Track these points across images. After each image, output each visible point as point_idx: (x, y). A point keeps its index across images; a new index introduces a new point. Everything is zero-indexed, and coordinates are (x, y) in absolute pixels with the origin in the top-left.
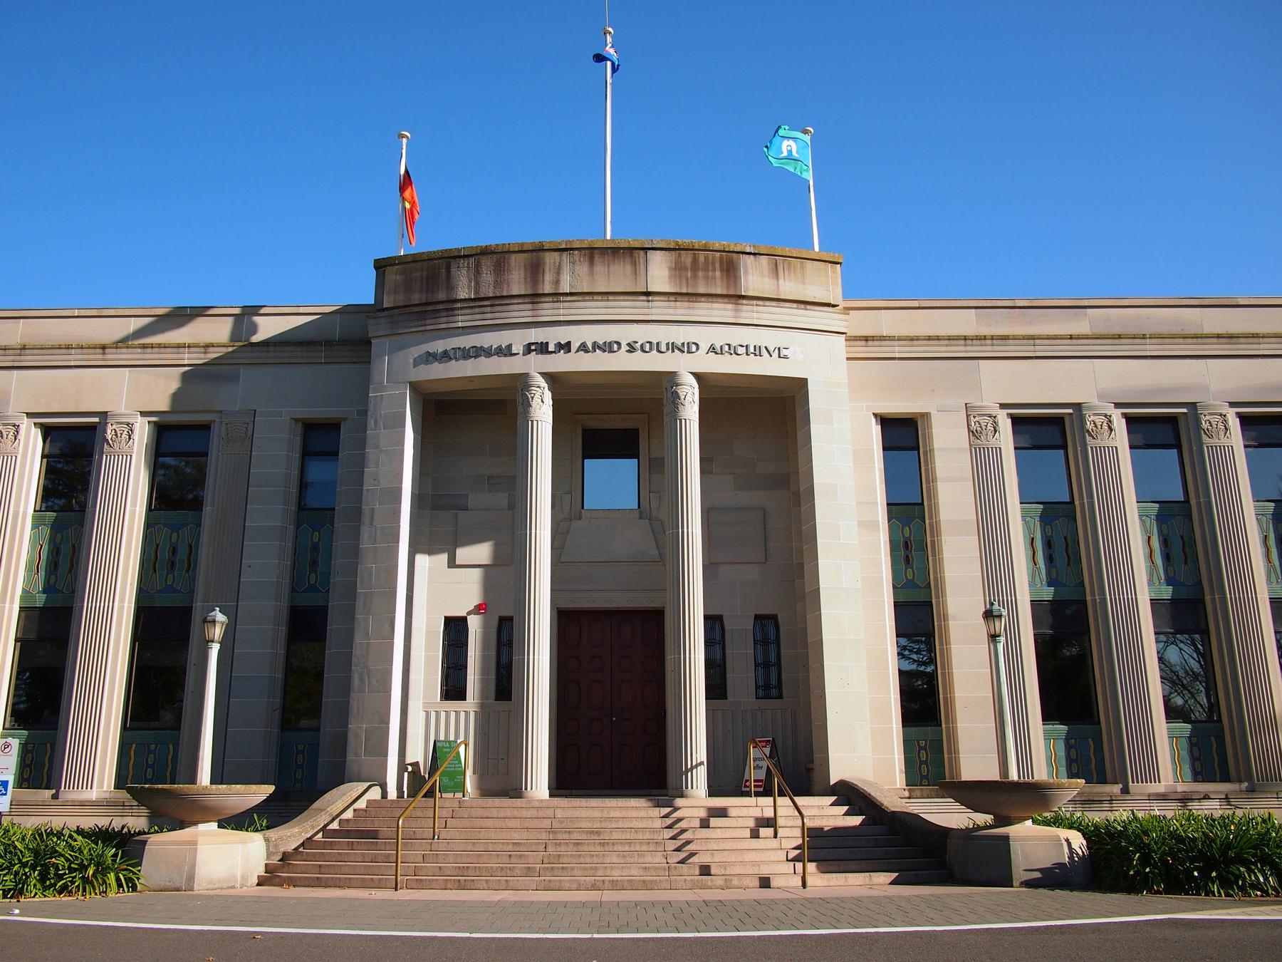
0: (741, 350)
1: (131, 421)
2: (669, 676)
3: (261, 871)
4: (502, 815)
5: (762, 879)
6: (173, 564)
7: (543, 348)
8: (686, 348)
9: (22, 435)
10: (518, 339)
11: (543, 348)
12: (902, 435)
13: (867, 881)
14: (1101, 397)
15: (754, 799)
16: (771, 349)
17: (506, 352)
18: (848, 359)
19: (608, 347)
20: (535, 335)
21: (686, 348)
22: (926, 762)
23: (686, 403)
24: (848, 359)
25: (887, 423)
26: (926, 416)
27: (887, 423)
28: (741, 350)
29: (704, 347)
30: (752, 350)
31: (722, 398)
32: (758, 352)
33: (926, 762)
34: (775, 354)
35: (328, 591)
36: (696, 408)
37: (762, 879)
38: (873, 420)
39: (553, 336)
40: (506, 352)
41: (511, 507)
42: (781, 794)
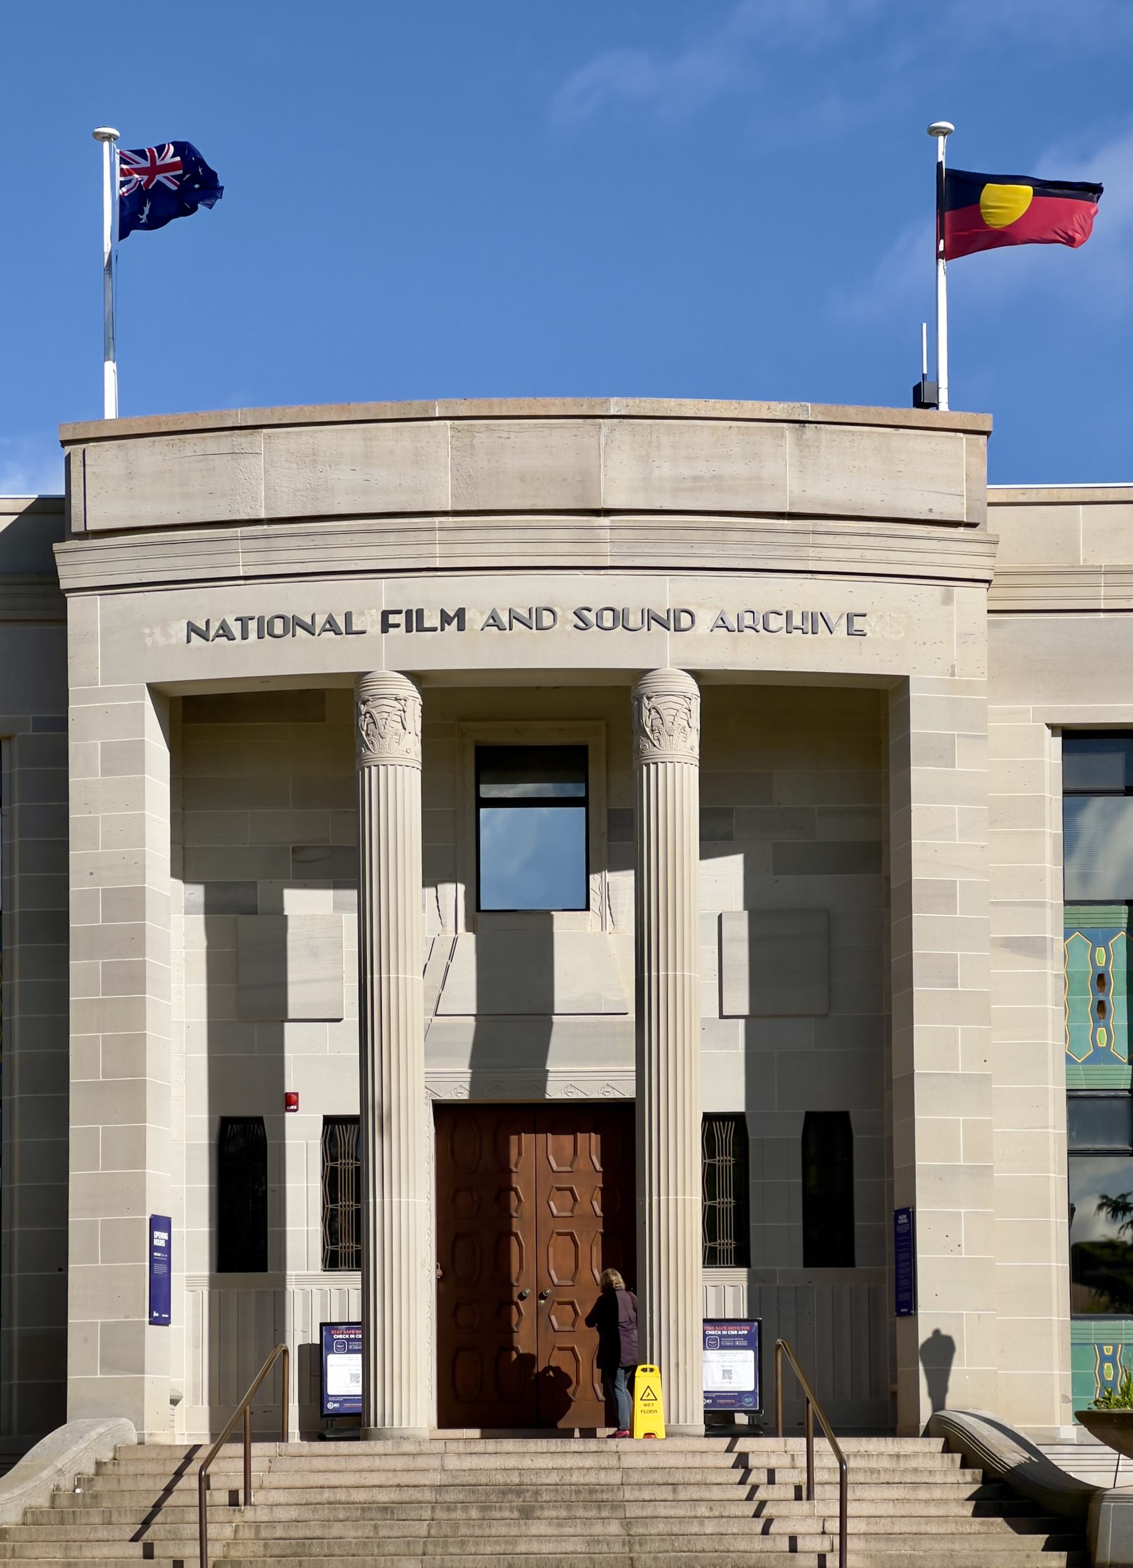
0: (776, 622)
2: (118, 208)
4: (354, 1466)
5: (730, 1372)
8: (671, 621)
10: (368, 599)
11: (415, 621)
13: (983, 1529)
17: (341, 627)
18: (989, 612)
19: (535, 619)
21: (671, 621)
22: (1112, 1359)
24: (989, 612)
28: (776, 622)
29: (706, 618)
30: (797, 621)
31: (738, 709)
33: (1112, 1359)
34: (841, 629)
36: (694, 739)
37: (730, 1372)
38: (1049, 732)
39: (432, 595)
40: (341, 627)
41: (909, 1260)
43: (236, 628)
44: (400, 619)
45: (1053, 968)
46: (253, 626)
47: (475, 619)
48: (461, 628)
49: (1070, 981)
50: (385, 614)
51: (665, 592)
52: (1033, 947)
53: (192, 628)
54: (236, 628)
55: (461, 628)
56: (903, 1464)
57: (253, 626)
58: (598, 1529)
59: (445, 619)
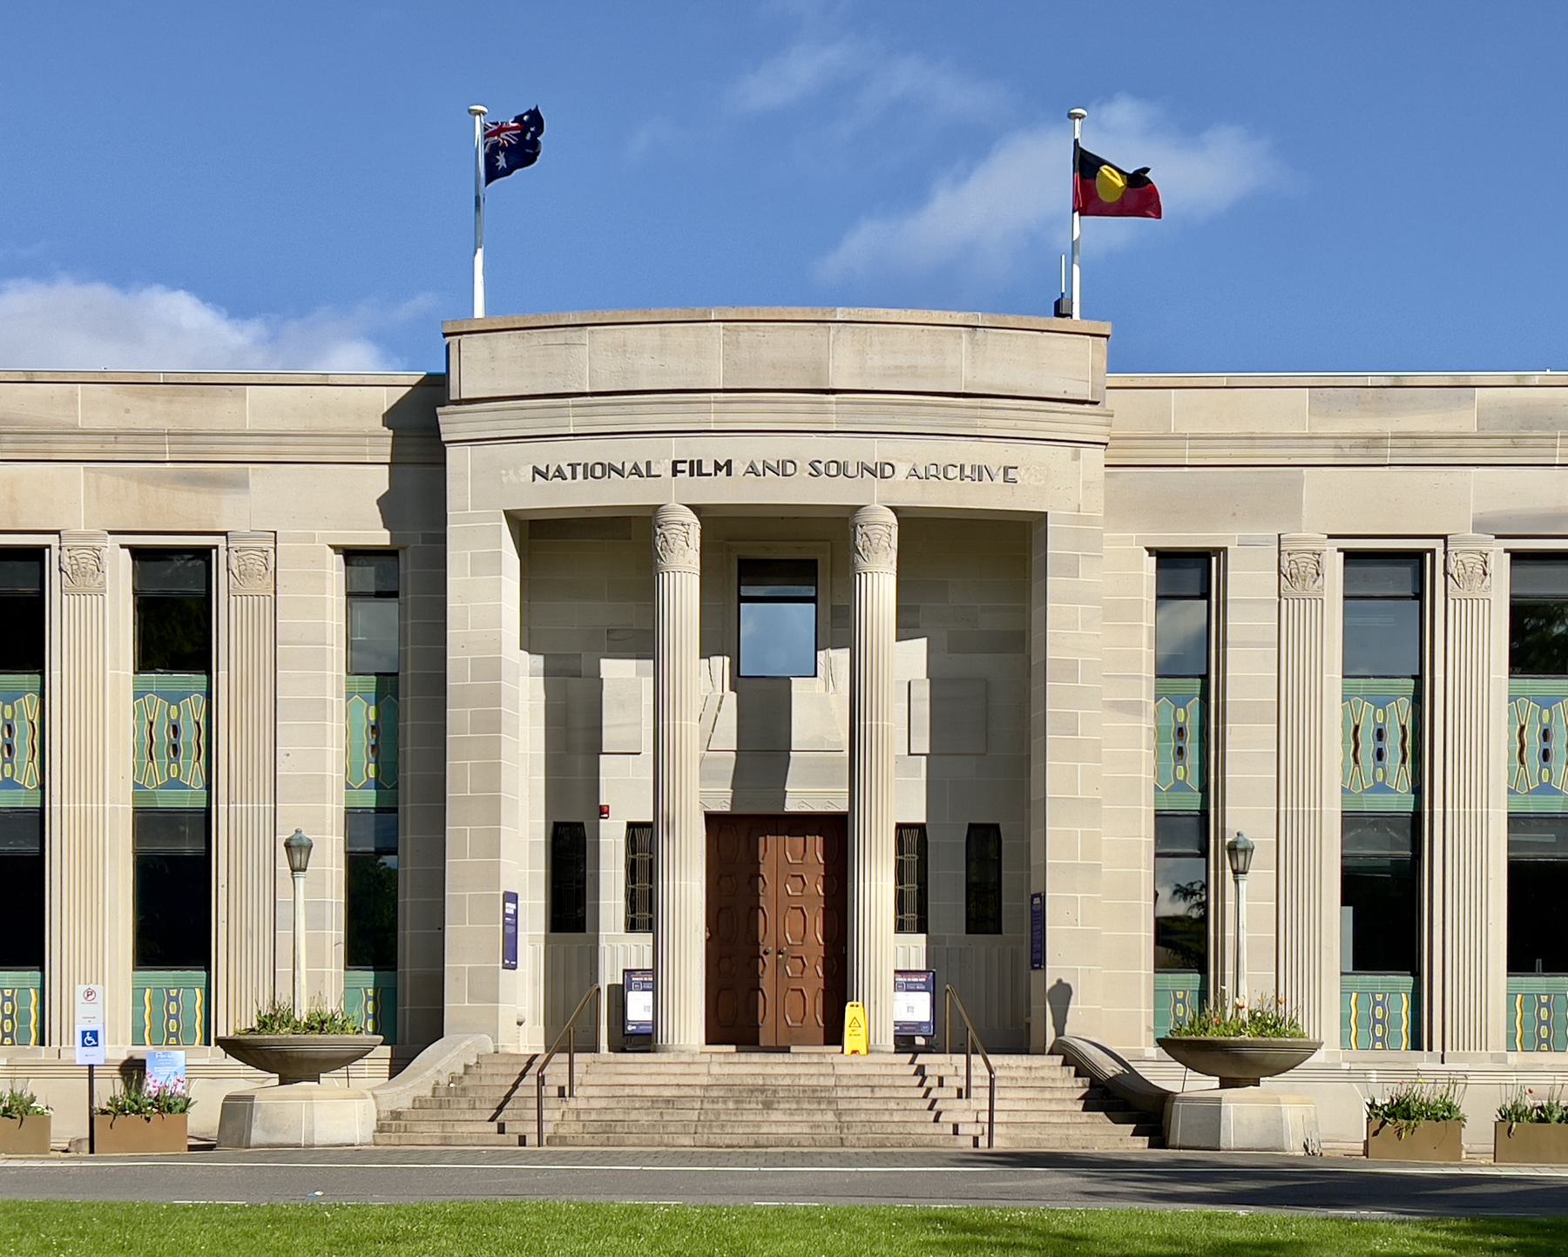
1: (97, 544)
3: (374, 1127)
6: (175, 749)
7: (696, 468)
8: (878, 471)
9: (106, 560)
11: (696, 468)
12: (1188, 572)
14: (1479, 526)
15: (948, 1056)
16: (994, 470)
20: (678, 448)
21: (878, 471)
23: (676, 548)
25: (1167, 558)
26: (1221, 552)
27: (1167, 558)
29: (903, 470)
30: (968, 471)
31: (923, 533)
32: (980, 472)
34: (999, 478)
35: (396, 787)
39: (709, 450)
42: (975, 1052)
43: (568, 472)
44: (686, 467)
45: (1147, 724)
46: (580, 469)
47: (739, 468)
48: (729, 474)
49: (1159, 733)
50: (675, 463)
51: (876, 450)
52: (1134, 708)
53: (536, 471)
54: (568, 472)
55: (729, 474)
56: (1034, 1074)
57: (580, 469)
58: (818, 1117)
59: (718, 467)
